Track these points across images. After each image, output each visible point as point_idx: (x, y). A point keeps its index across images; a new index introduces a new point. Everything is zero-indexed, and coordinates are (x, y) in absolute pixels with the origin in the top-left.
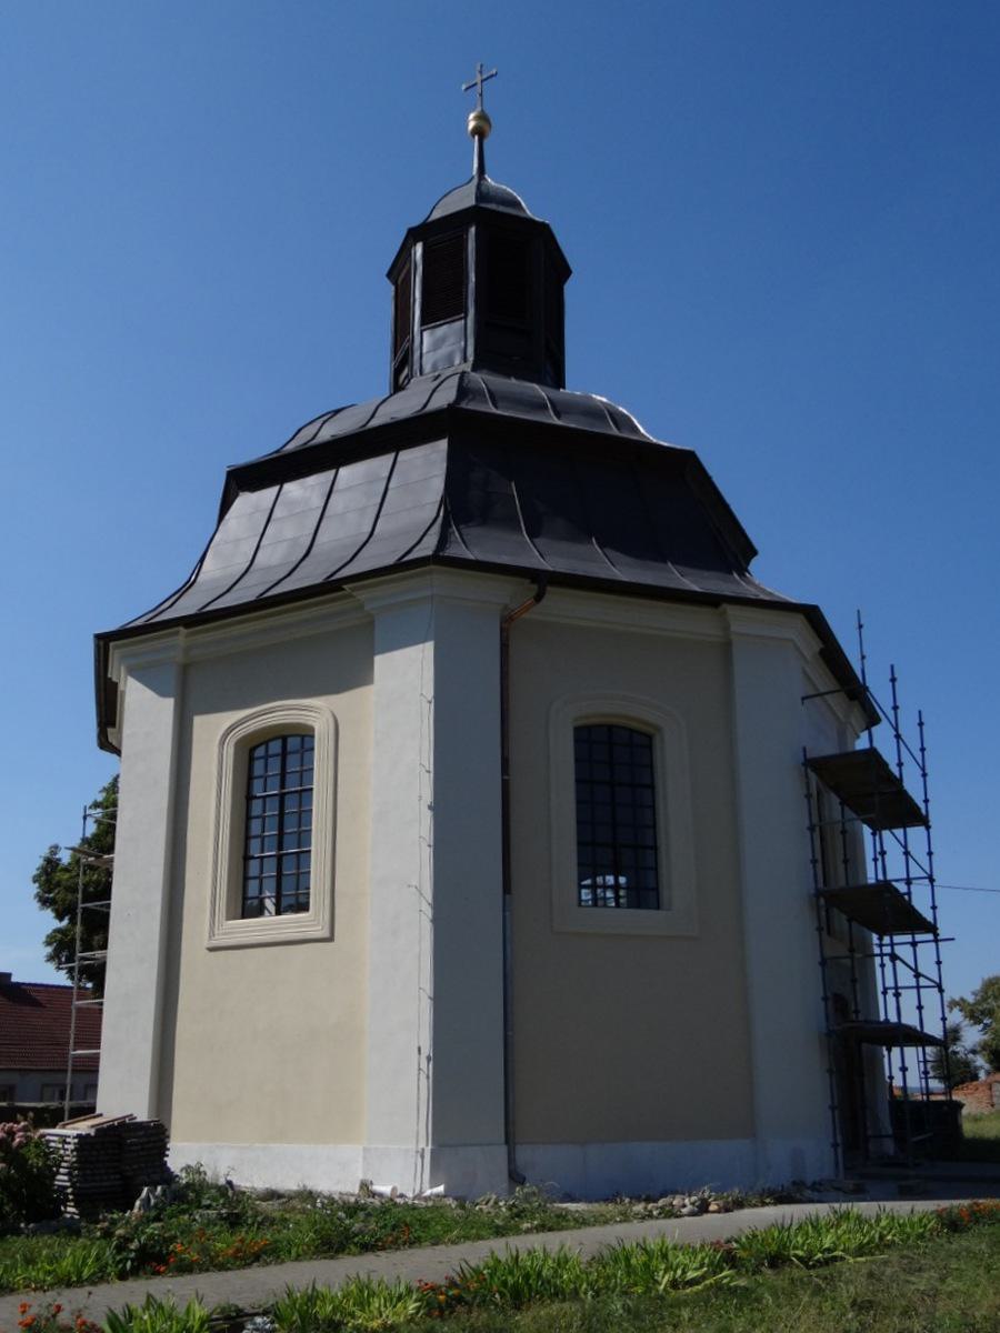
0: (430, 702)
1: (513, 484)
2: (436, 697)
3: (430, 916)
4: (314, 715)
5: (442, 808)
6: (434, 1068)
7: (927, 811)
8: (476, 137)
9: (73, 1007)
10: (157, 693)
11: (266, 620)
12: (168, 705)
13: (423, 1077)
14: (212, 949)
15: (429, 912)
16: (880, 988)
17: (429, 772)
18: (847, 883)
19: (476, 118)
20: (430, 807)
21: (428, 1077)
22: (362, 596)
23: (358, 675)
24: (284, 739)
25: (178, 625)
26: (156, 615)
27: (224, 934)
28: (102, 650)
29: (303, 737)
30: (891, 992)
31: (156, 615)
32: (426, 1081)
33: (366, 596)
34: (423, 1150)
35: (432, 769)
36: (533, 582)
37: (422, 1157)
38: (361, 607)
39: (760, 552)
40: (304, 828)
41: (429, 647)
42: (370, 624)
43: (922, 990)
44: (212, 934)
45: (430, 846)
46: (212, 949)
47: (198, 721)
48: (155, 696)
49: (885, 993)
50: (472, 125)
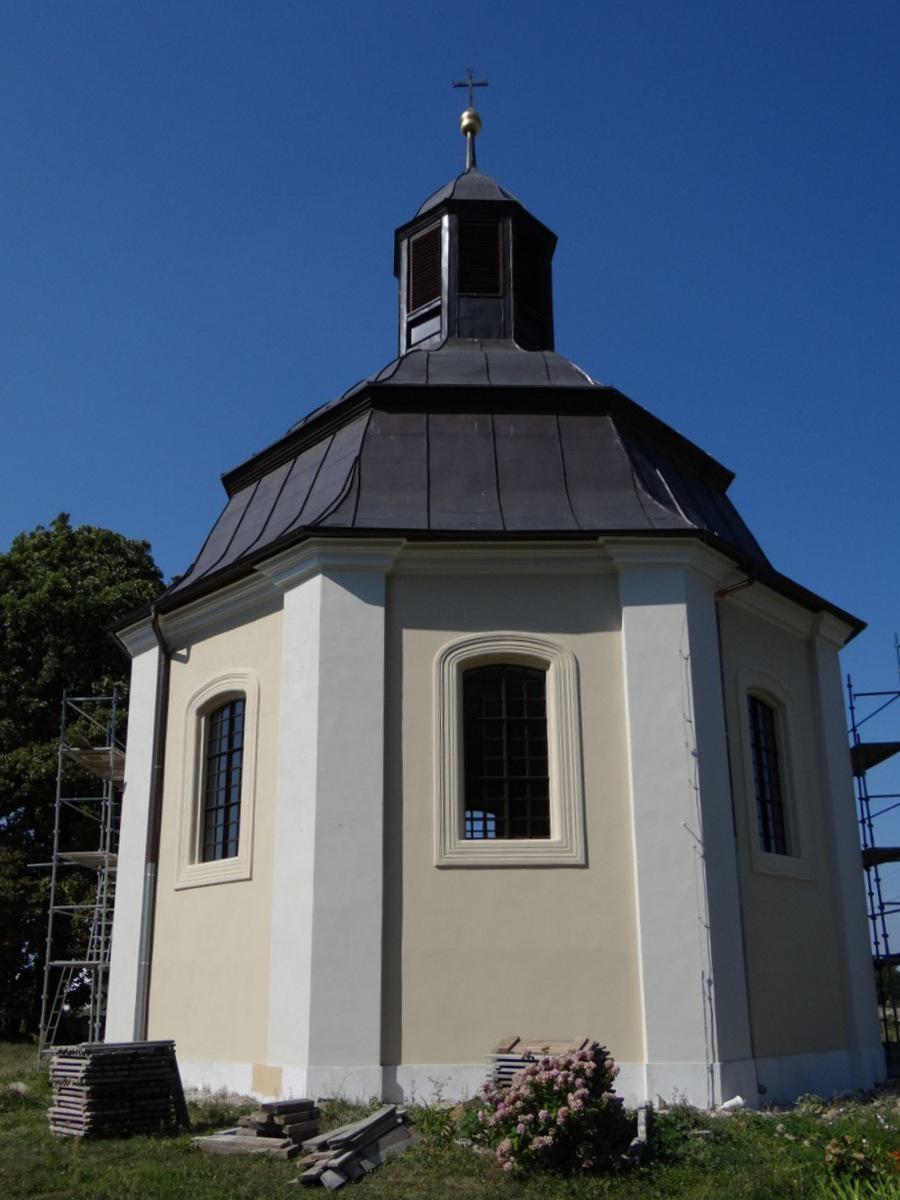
0: (687, 659)
1: (658, 472)
2: (691, 654)
3: (701, 852)
6: (716, 989)
8: (469, 134)
9: (50, 912)
10: (363, 600)
12: (378, 613)
13: (707, 1003)
14: (440, 867)
15: (700, 849)
17: (690, 722)
19: (469, 117)
20: (693, 754)
21: (710, 999)
22: (612, 550)
23: (607, 620)
25: (402, 537)
27: (456, 853)
30: (879, 919)
33: (621, 553)
34: (712, 1065)
35: (693, 720)
36: (741, 568)
37: (712, 1072)
39: (219, 478)
42: (614, 576)
43: (885, 916)
44: (443, 851)
46: (440, 867)
47: (410, 637)
48: (362, 602)
49: (874, 917)
50: (465, 122)
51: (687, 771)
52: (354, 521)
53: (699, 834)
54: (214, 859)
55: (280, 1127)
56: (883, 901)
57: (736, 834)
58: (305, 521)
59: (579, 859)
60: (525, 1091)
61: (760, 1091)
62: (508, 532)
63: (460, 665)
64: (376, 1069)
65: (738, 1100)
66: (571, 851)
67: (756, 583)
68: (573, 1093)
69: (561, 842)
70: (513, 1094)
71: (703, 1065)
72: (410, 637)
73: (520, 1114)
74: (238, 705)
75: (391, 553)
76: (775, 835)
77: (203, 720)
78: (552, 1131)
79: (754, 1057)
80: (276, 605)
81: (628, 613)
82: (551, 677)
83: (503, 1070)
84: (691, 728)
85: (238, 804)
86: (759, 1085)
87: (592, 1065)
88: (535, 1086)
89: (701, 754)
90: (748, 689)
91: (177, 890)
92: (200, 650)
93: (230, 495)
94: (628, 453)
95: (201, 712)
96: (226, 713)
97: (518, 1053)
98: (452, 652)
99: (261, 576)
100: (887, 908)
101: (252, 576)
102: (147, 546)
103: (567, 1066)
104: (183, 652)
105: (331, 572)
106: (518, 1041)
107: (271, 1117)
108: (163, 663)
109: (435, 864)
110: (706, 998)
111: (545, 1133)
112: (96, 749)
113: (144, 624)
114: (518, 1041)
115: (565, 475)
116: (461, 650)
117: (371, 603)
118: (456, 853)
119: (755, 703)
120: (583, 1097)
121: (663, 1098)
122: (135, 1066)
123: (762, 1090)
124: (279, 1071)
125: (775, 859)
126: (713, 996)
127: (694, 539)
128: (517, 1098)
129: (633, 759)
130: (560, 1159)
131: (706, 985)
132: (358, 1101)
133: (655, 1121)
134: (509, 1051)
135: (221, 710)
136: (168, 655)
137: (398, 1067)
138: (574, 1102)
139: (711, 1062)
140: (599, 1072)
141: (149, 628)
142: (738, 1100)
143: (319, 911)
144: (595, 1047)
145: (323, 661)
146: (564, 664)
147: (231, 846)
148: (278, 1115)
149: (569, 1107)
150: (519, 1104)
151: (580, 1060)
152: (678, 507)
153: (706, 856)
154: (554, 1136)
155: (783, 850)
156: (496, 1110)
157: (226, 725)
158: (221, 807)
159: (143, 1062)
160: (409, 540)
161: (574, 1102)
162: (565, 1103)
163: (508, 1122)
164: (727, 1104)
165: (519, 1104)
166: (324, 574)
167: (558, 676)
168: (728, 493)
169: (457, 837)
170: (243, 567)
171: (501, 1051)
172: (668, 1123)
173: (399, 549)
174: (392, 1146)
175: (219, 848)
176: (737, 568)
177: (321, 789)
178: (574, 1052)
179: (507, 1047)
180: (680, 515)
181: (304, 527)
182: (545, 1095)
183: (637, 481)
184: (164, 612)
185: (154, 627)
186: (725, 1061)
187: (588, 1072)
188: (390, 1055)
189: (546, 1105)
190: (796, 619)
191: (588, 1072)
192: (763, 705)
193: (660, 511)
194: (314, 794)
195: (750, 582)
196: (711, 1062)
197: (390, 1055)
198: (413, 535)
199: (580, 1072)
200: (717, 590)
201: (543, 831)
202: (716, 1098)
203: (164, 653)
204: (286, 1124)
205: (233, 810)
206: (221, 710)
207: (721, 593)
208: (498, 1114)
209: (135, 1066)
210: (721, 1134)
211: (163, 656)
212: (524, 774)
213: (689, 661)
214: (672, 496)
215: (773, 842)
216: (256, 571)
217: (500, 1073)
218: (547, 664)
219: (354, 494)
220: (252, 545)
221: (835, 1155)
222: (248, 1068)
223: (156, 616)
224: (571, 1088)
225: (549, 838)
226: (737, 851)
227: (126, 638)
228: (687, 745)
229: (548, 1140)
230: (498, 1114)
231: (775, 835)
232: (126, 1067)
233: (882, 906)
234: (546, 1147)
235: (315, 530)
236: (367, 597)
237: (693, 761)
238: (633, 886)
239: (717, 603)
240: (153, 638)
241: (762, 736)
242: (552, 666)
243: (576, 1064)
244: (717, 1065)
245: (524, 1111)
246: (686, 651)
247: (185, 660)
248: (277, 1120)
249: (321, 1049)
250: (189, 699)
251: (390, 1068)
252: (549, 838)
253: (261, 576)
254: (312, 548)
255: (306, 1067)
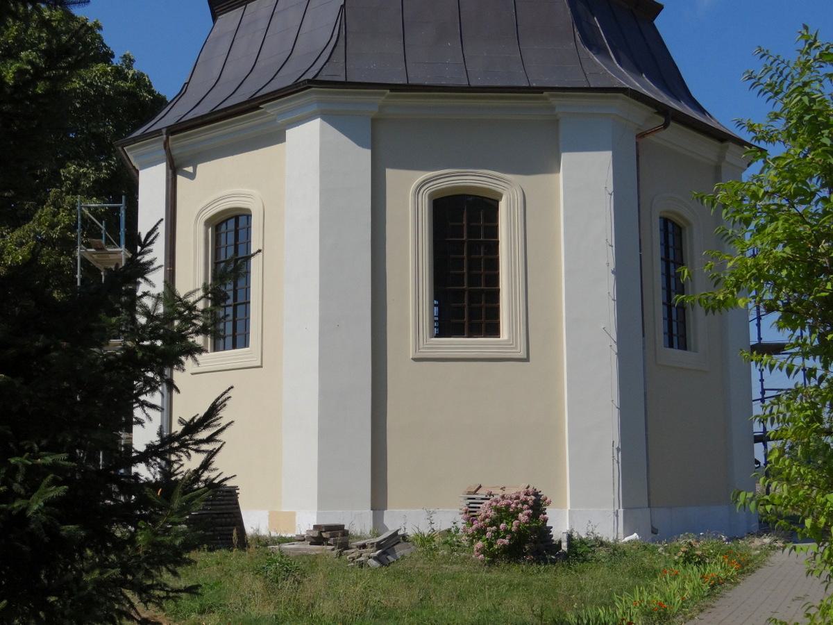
0: (611, 195)
1: (595, 19)
4: (506, 185)
5: (620, 272)
7: (154, 269)
11: (501, 101)
12: (367, 154)
13: (616, 465)
14: (415, 360)
15: (615, 347)
16: (756, 394)
18: (760, 339)
20: (613, 272)
21: (618, 462)
22: (555, 102)
23: (548, 164)
24: (237, 218)
26: (148, 128)
27: (429, 348)
28: (199, 121)
29: (237, 218)
31: (148, 128)
32: (617, 465)
33: (560, 104)
34: (617, 511)
35: (614, 245)
36: (659, 113)
37: (617, 516)
38: (553, 108)
40: (474, 272)
41: (606, 157)
42: (555, 122)
44: (417, 347)
45: (614, 300)
46: (415, 360)
47: (392, 175)
51: (608, 285)
52: (346, 77)
53: (615, 336)
54: (224, 349)
55: (326, 539)
56: (765, 387)
57: (644, 336)
58: (310, 76)
59: (522, 354)
60: (492, 514)
61: (652, 532)
62: (472, 87)
63: (431, 196)
64: (369, 513)
65: (635, 536)
66: (516, 348)
67: (672, 124)
68: (522, 513)
69: (508, 340)
70: (483, 515)
71: (610, 510)
72: (392, 175)
73: (489, 526)
74: (242, 221)
75: (373, 103)
76: (677, 335)
77: (210, 229)
78: (508, 537)
79: (649, 506)
80: (279, 137)
81: (566, 157)
82: (503, 206)
83: (471, 505)
84: (611, 252)
85: (247, 303)
86: (652, 527)
87: (533, 497)
88: (498, 510)
89: (619, 272)
90: (661, 212)
91: (192, 374)
92: (205, 169)
93: (214, 19)
94: (570, 7)
95: (208, 223)
96: (231, 224)
97: (482, 493)
98: (425, 184)
99: (267, 113)
100: (768, 394)
101: (258, 111)
102: (133, 61)
103: (518, 498)
104: (190, 169)
105: (331, 117)
106: (480, 487)
107: (320, 533)
108: (170, 177)
109: (411, 357)
110: (615, 462)
111: (504, 537)
112: (109, 250)
113: (156, 141)
114: (480, 487)
115: (517, 25)
116: (431, 184)
117: (359, 146)
118: (429, 348)
119: (665, 221)
120: (528, 515)
121: (580, 534)
122: (214, 503)
123: (654, 531)
124: (294, 514)
125: (676, 353)
126: (620, 461)
127: (621, 95)
128: (486, 517)
129: (566, 276)
130: (514, 553)
131: (615, 452)
132: (361, 533)
133: (572, 540)
134: (475, 493)
135: (226, 221)
136: (174, 170)
137: (385, 512)
138: (523, 517)
139: (617, 508)
140: (538, 506)
141: (161, 145)
142: (635, 536)
143: (324, 394)
144: (536, 494)
145: (323, 192)
146: (514, 197)
147: (240, 339)
148: (325, 532)
149: (520, 521)
150: (487, 520)
151: (525, 495)
152: (611, 53)
153: (619, 354)
154: (510, 540)
155: (684, 346)
156: (473, 524)
157: (231, 236)
158: (230, 306)
159: (219, 500)
160: (392, 90)
161: (523, 517)
162: (517, 518)
163: (481, 532)
164: (627, 539)
165: (487, 520)
166: (324, 119)
167: (509, 206)
168: (656, 22)
169: (428, 336)
170: (252, 105)
171: (469, 493)
172: (582, 542)
173: (383, 98)
174: (400, 550)
175: (229, 340)
176: (655, 113)
177: (323, 296)
178: (777, 116)
179: (474, 490)
180: (614, 63)
181: (308, 80)
182: (505, 513)
183: (577, 34)
184: (173, 133)
185: (165, 148)
186: (627, 509)
187: (530, 502)
188: (379, 502)
189: (505, 521)
190: (706, 149)
191: (530, 502)
192: (674, 223)
193: (596, 65)
194: (318, 302)
195: (666, 126)
196: (617, 508)
197: (379, 502)
198: (395, 88)
199: (525, 502)
200: (639, 132)
201: (494, 330)
202: (619, 535)
203: (171, 168)
204: (331, 537)
205: (240, 309)
206: (226, 221)
207: (641, 136)
208: (474, 527)
209: (214, 503)
210: (616, 551)
211: (170, 171)
212: (486, 302)
213: (612, 196)
214: (606, 41)
215: (675, 339)
216: (262, 108)
217: (470, 507)
218: (501, 195)
219: (341, 43)
220: (260, 90)
221: (683, 552)
222: (265, 514)
223: (168, 138)
224: (521, 510)
225: (499, 337)
226: (644, 348)
227: (133, 155)
228: (608, 264)
229: (506, 541)
230: (474, 527)
231: (677, 335)
232: (210, 503)
233: (763, 392)
234: (504, 545)
235: (314, 82)
236: (360, 143)
237: (613, 277)
238: (563, 364)
239: (637, 144)
240: (163, 153)
241: (671, 251)
242: (504, 198)
243: (522, 497)
244: (621, 511)
245: (491, 525)
246: (611, 189)
247: (192, 176)
248: (324, 535)
249: (325, 499)
250: (196, 213)
251: (377, 511)
252: (499, 337)
253: (265, 113)
254: (311, 98)
255: (316, 510)
